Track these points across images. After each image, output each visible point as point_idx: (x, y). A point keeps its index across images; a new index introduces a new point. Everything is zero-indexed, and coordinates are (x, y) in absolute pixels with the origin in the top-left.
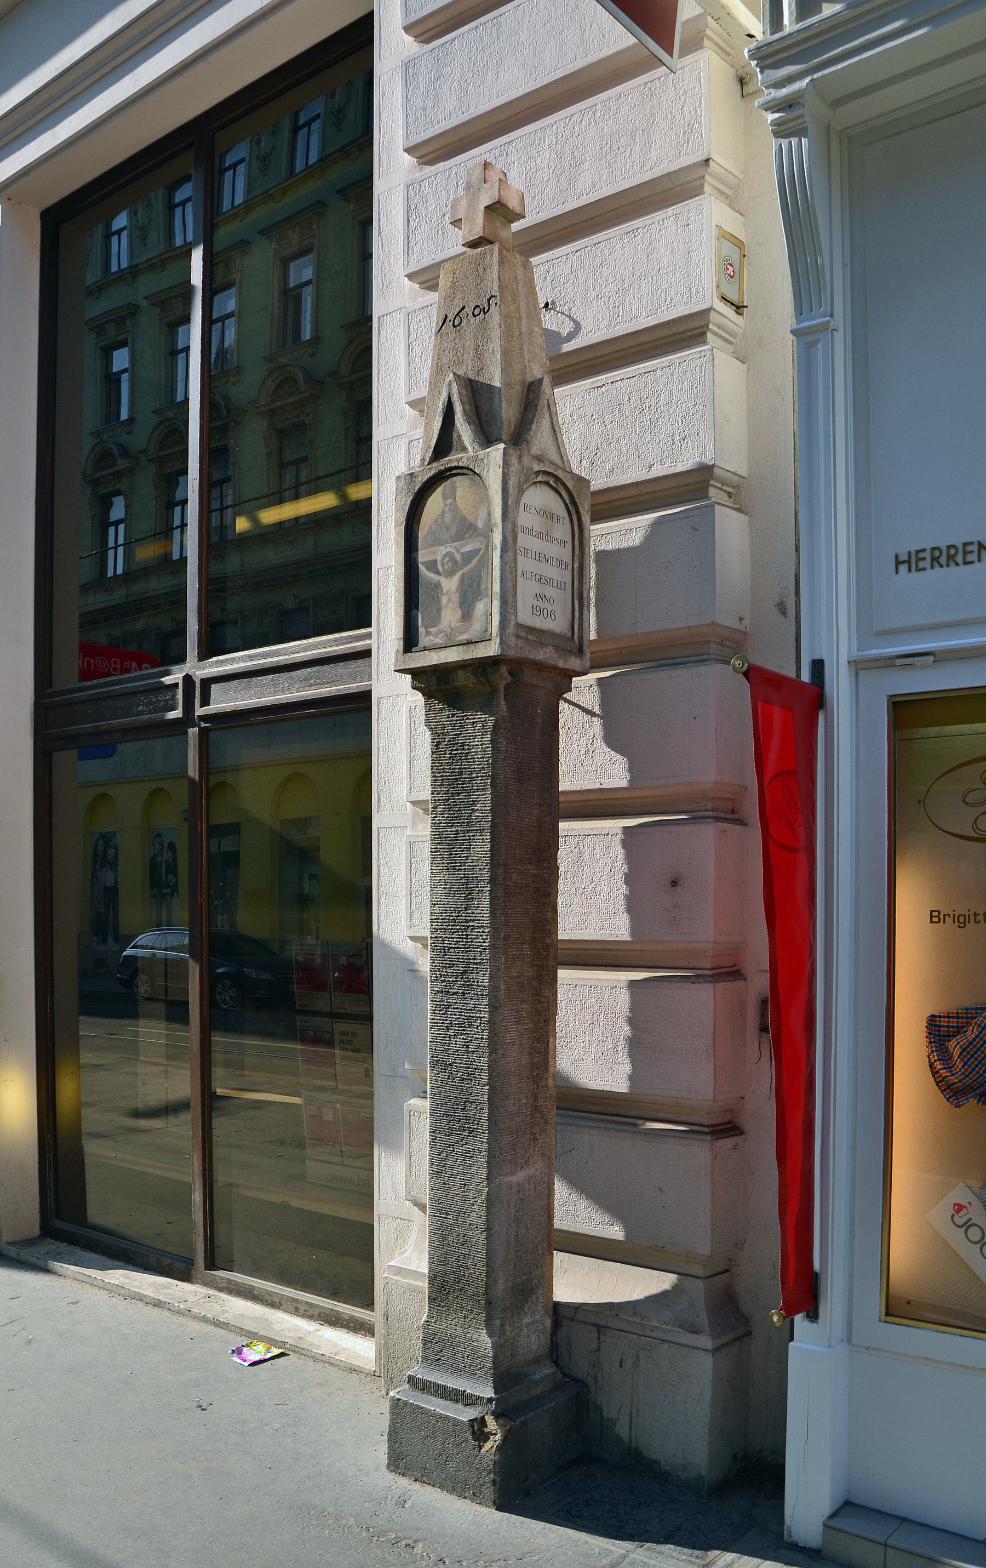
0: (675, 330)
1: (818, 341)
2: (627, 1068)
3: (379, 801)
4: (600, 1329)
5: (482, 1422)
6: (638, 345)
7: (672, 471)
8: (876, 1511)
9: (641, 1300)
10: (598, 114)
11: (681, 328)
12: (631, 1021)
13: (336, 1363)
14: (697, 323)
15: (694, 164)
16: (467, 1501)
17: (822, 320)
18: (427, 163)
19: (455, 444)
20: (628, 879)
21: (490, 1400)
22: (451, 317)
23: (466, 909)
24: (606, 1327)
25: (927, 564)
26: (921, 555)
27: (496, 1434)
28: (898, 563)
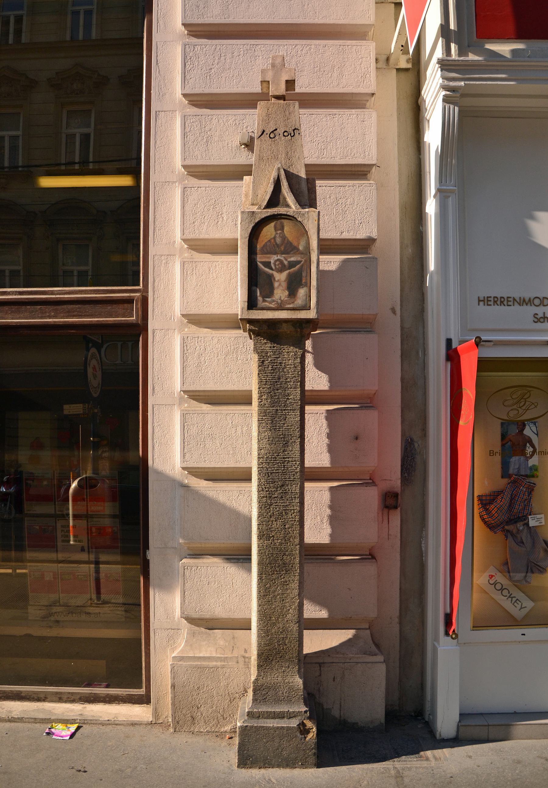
0: (353, 169)
1: (449, 196)
2: (329, 531)
3: (153, 389)
4: (320, 665)
5: (303, 724)
6: (331, 171)
7: (354, 237)
8: (469, 714)
9: (337, 646)
11: (359, 169)
12: (331, 507)
13: (120, 723)
14: (365, 169)
15: (367, 93)
16: (297, 769)
17: (452, 188)
18: (193, 36)
19: (281, 201)
20: (329, 436)
21: (306, 712)
22: (268, 131)
23: (284, 451)
24: (324, 663)
25: (492, 303)
26: (489, 299)
27: (312, 728)
28: (479, 301)
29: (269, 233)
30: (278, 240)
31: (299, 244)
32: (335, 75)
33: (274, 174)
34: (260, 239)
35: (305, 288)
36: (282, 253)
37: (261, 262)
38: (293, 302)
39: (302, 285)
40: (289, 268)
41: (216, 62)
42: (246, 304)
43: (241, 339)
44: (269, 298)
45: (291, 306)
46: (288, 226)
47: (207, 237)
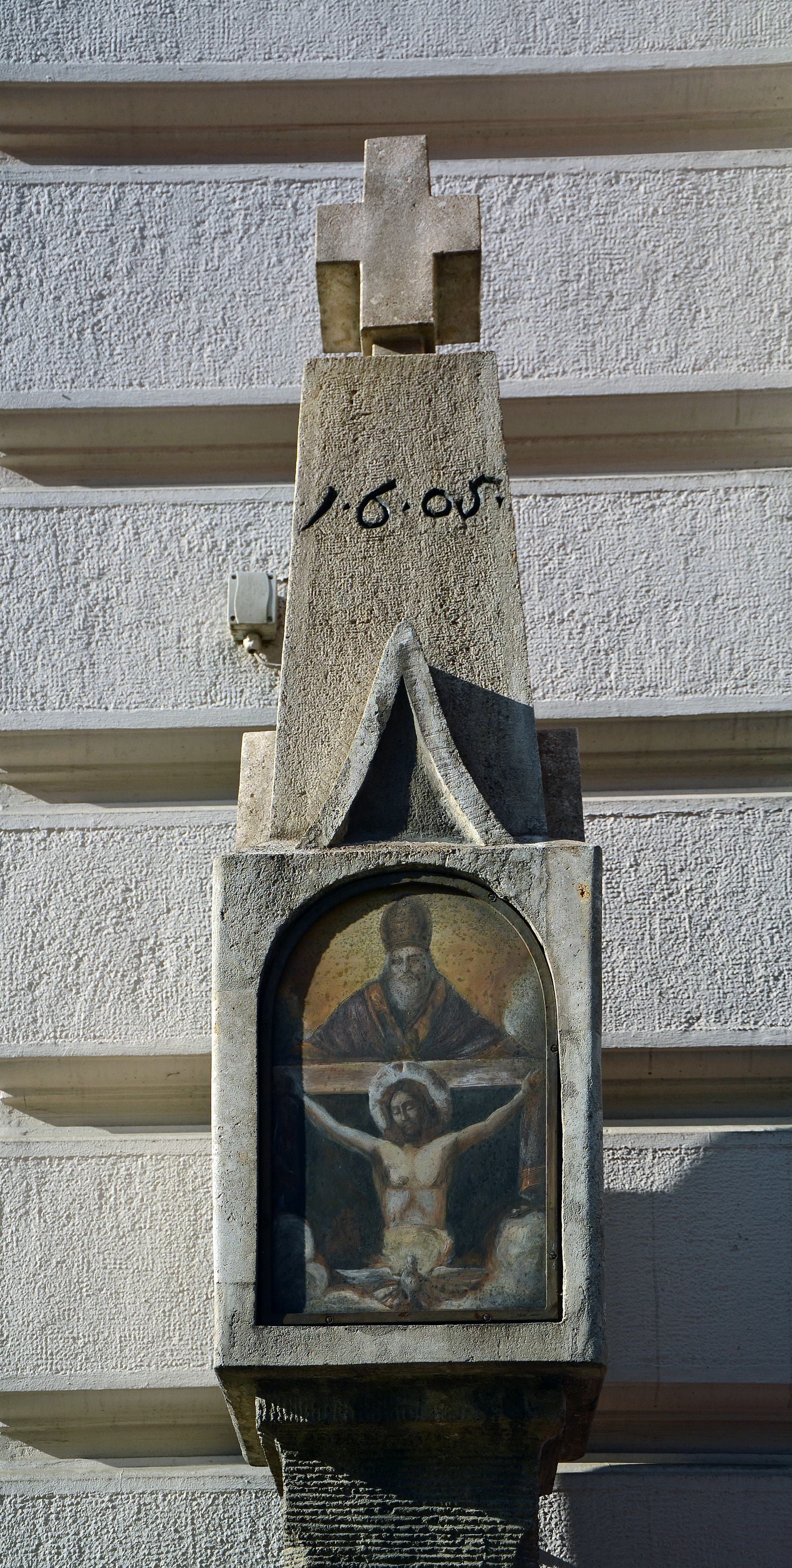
6: (638, 754)
7: (745, 1040)
10: (556, 200)
11: (756, 740)
19: (416, 810)
22: (351, 494)
29: (356, 960)
30: (403, 992)
31: (500, 1007)
32: (660, 311)
33: (381, 679)
34: (319, 987)
35: (532, 1219)
36: (422, 1053)
37: (322, 1099)
38: (476, 1287)
39: (518, 1202)
40: (457, 1124)
41: (123, 262)
42: (250, 1296)
43: (244, 1499)
44: (360, 1266)
45: (466, 1303)
46: (449, 930)
47: (88, 1048)
